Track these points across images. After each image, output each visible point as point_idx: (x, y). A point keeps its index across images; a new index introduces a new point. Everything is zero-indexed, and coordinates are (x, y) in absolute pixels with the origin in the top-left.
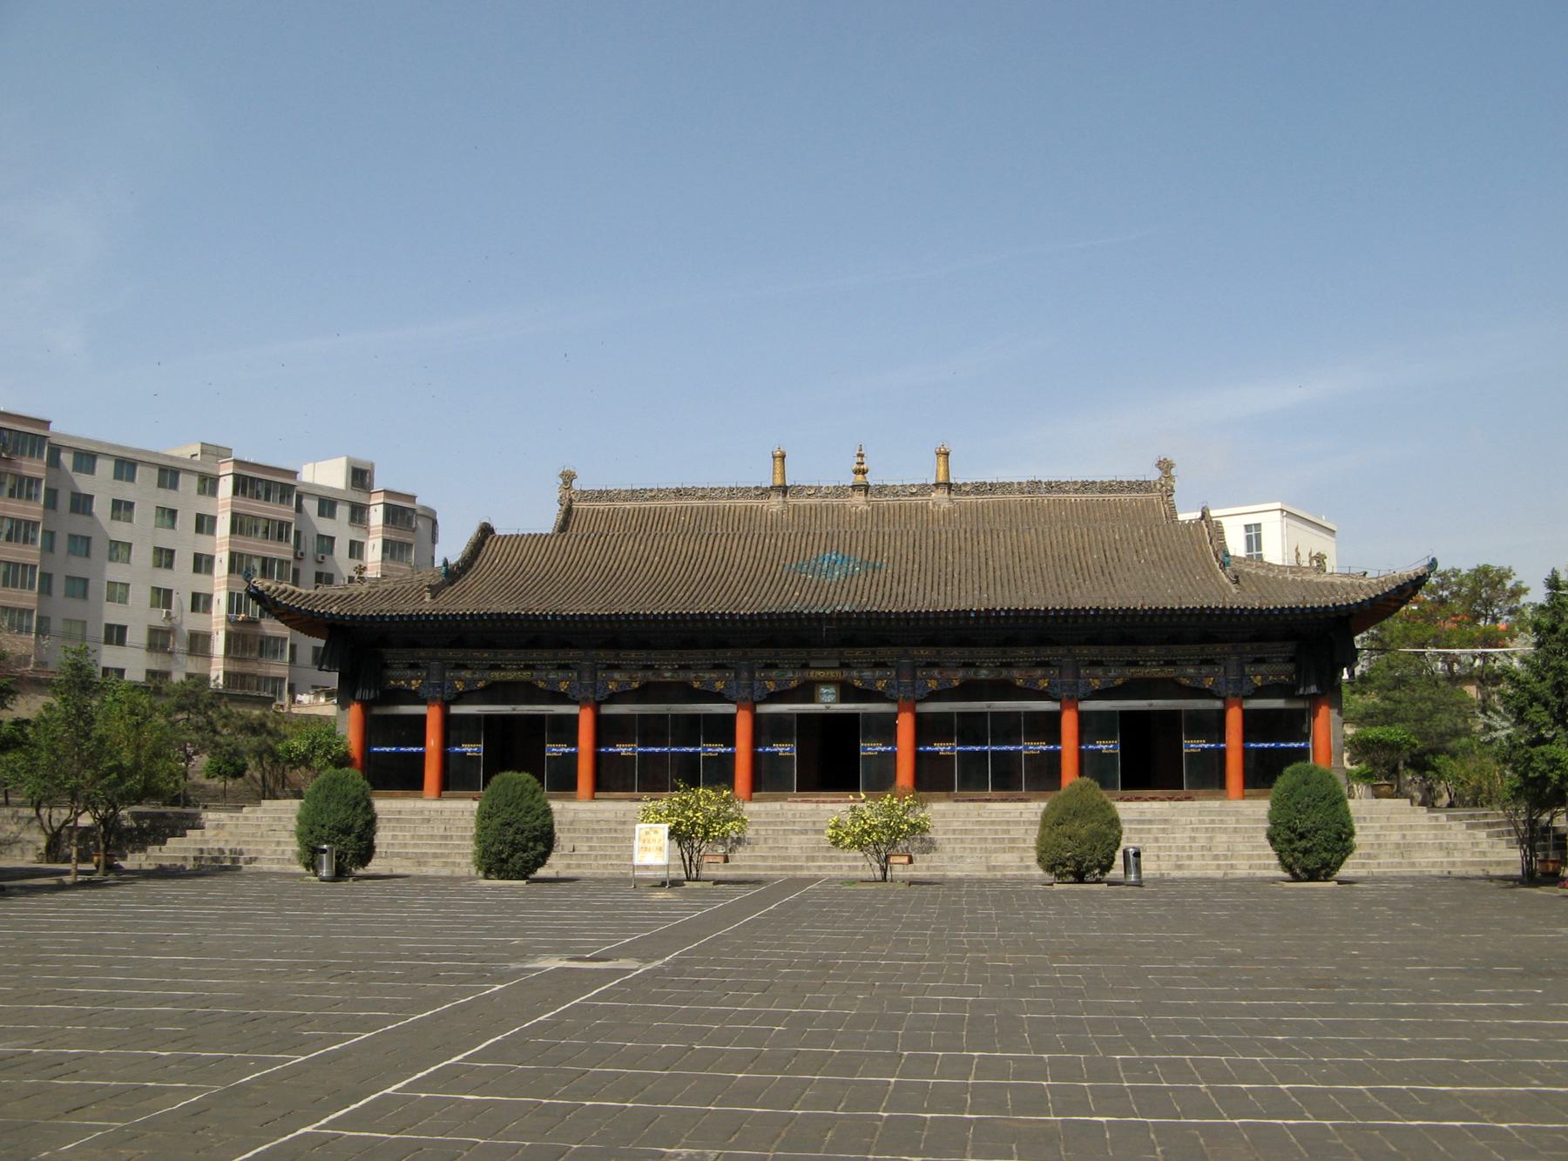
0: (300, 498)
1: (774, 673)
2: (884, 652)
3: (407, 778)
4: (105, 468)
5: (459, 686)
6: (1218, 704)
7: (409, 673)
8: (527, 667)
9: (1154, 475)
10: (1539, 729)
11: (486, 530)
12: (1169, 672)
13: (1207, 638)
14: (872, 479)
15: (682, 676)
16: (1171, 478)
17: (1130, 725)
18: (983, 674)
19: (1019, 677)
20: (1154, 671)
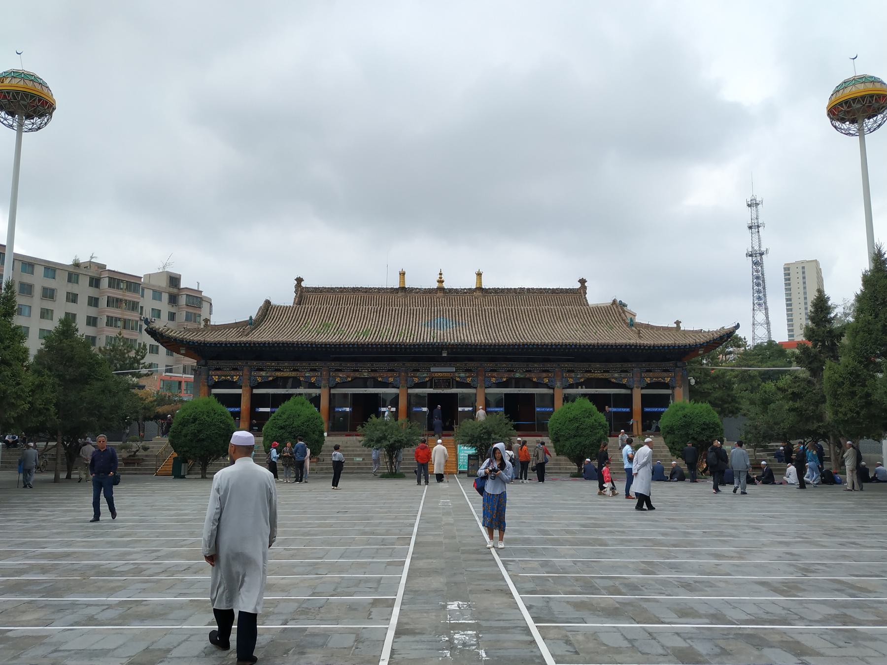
0: (143, 290)
1: (573, 375)
2: (471, 365)
3: (621, 423)
4: (39, 271)
5: (259, 379)
6: (551, 391)
8: (294, 370)
9: (578, 286)
11: (268, 303)
12: (606, 376)
13: (625, 360)
14: (446, 285)
15: (372, 375)
16: (585, 288)
17: (432, 400)
18: (518, 375)
19: (615, 376)
20: (599, 375)
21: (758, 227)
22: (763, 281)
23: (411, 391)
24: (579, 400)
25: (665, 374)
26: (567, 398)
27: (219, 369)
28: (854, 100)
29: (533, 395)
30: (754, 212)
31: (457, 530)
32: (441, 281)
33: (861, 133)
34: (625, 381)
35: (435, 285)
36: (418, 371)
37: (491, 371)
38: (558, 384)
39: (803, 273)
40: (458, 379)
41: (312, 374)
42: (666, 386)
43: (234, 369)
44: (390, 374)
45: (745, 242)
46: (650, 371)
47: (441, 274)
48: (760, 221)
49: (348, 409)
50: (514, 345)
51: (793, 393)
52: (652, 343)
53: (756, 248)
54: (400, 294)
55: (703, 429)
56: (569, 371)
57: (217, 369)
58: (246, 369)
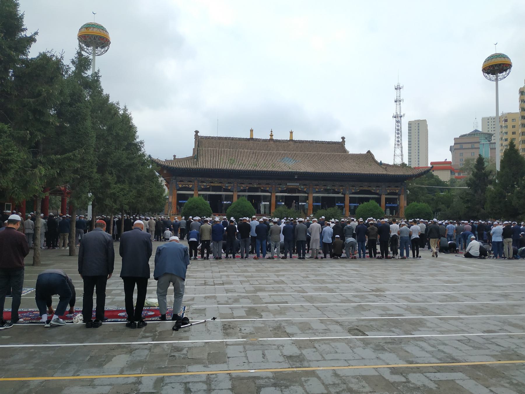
1: (354, 188)
2: (307, 182)
5: (202, 187)
6: (307, 195)
7: (189, 183)
8: (220, 183)
9: (341, 140)
10: (193, 245)
14: (274, 138)
15: (259, 186)
16: (345, 142)
19: (373, 189)
20: (366, 188)
21: (400, 101)
22: (401, 132)
23: (200, 193)
24: (371, 201)
25: (396, 188)
26: (239, 196)
27: (182, 181)
28: (496, 65)
29: (260, 196)
30: (398, 93)
32: (271, 136)
34: (378, 191)
35: (269, 138)
36: (281, 184)
38: (348, 192)
39: (418, 127)
41: (229, 185)
42: (395, 194)
43: (189, 181)
44: (267, 186)
45: (393, 109)
46: (390, 187)
49: (225, 202)
51: (468, 200)
53: (398, 113)
54: (251, 142)
55: (426, 215)
56: (353, 186)
57: (180, 181)
58: (196, 181)
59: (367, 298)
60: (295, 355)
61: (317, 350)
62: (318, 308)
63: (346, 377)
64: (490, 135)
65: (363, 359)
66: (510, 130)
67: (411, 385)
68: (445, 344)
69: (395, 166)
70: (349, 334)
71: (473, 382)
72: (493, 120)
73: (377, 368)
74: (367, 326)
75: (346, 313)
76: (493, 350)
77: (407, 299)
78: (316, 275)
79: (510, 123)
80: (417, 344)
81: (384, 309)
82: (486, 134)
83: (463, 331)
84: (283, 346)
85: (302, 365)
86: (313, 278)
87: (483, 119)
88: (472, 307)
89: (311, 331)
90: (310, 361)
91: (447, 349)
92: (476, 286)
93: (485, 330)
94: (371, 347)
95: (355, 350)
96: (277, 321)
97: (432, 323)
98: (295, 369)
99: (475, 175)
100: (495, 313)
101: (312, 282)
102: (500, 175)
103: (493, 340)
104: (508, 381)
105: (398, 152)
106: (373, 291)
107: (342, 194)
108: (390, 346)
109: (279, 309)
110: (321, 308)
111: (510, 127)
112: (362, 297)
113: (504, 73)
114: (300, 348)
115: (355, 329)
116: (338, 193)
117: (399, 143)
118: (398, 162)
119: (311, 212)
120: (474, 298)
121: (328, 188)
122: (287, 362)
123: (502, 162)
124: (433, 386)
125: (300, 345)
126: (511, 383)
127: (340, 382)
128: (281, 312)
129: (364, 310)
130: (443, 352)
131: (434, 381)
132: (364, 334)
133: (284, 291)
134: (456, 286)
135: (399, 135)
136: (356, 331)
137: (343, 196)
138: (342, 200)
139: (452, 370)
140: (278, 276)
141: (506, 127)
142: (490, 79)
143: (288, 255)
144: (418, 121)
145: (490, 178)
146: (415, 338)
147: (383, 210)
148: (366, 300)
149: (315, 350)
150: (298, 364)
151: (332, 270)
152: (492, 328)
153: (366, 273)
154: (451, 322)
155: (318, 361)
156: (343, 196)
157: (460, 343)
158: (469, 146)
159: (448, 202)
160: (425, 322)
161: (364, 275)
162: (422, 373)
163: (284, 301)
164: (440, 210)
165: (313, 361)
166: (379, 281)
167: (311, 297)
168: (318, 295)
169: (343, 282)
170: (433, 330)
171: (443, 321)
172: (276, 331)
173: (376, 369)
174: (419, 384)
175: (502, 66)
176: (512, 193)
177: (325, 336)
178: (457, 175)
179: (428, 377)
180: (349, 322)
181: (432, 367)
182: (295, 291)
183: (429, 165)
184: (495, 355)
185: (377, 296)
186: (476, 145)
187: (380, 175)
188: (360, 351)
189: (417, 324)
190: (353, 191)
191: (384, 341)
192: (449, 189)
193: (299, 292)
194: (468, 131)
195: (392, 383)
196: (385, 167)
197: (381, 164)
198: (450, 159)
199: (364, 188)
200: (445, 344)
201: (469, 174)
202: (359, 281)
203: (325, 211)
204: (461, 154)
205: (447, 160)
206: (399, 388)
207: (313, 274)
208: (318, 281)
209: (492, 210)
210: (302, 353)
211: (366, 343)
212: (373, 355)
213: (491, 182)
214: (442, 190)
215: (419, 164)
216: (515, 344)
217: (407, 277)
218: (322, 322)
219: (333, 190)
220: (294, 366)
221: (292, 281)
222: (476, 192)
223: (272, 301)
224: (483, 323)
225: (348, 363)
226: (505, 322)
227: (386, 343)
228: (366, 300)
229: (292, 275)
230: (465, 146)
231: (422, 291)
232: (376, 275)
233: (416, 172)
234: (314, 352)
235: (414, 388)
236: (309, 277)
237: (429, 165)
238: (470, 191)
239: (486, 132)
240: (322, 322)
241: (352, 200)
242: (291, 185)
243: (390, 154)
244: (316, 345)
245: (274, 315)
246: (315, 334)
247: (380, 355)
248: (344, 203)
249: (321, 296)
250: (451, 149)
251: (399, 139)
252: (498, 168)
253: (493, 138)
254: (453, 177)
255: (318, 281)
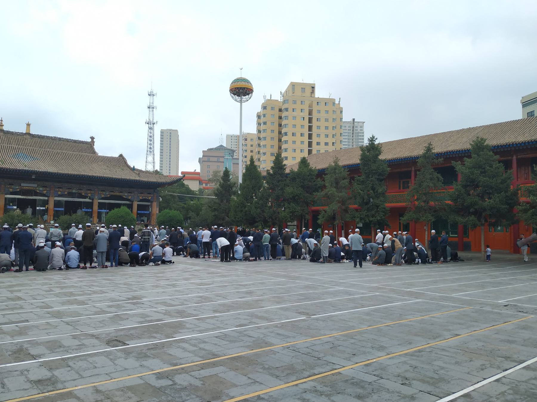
1: (104, 193)
6: (46, 198)
9: (90, 140)
19: (125, 195)
20: (118, 194)
21: (153, 108)
24: (122, 207)
25: (149, 195)
28: (241, 88)
29: (36, 200)
30: (151, 99)
31: (501, 183)
33: (241, 102)
34: (130, 198)
36: (13, 185)
37: (58, 188)
38: (96, 197)
40: (38, 191)
42: (148, 201)
46: (142, 193)
47: (2, 121)
48: (154, 105)
50: (100, 177)
52: (165, 181)
56: (102, 191)
59: (124, 307)
60: (45, 378)
61: (72, 369)
62: (68, 323)
63: (109, 391)
64: (233, 151)
65: (126, 369)
66: (249, 148)
67: (178, 387)
68: (205, 342)
69: (147, 172)
70: (108, 347)
71: (232, 373)
72: (235, 138)
73: (141, 376)
74: (127, 336)
75: (101, 325)
76: (247, 342)
77: (164, 303)
78: (62, 288)
79: (249, 143)
80: (179, 346)
81: (144, 316)
82: (230, 150)
83: (219, 328)
84: (29, 371)
85: (55, 387)
86: (58, 291)
87: (227, 136)
88: (224, 305)
89: (62, 349)
90: (65, 382)
91: (207, 347)
92: (226, 286)
93: (238, 324)
94: (133, 356)
95: (116, 362)
96: (17, 344)
97: (191, 324)
98: (47, 394)
99: (222, 186)
100: (244, 309)
101: (57, 295)
102: (242, 187)
103: (245, 333)
104: (262, 366)
105: (150, 159)
106: (129, 299)
107: (90, 199)
108: (152, 352)
109: (17, 329)
110: (72, 322)
111: (249, 145)
112: (118, 307)
113: (247, 97)
114: (50, 369)
115: (113, 340)
116: (85, 197)
117: (152, 150)
118: (150, 168)
119: (52, 218)
120: (225, 298)
121: (74, 191)
122: (35, 387)
123: (244, 175)
124: (198, 383)
125: (50, 366)
126: (264, 368)
127: (103, 397)
128: (21, 332)
129: (122, 319)
130: (204, 349)
131: (199, 378)
132: (125, 344)
133: (21, 308)
134: (209, 287)
135: (152, 142)
136: (115, 342)
137: (91, 201)
138: (90, 205)
139: (214, 365)
140: (12, 292)
141: (246, 145)
142: (236, 100)
143: (24, 268)
144: (170, 130)
145: (234, 189)
146: (176, 340)
147: (135, 216)
148: (123, 309)
149: (69, 369)
150: (50, 388)
151: (81, 281)
152: (243, 322)
153: (120, 282)
154: (208, 321)
155: (74, 380)
156: (91, 201)
157: (218, 339)
158: (215, 159)
159: (197, 210)
160: (184, 324)
161: (117, 284)
162: (187, 373)
163: (23, 319)
164: (190, 218)
165: (68, 381)
166: (134, 289)
167: (59, 312)
168: (66, 309)
169: (95, 292)
170: (193, 331)
171: (200, 321)
172: (17, 355)
173: (141, 378)
174: (185, 384)
175: (246, 89)
176: (251, 204)
177: (80, 352)
178: (204, 185)
179: (193, 376)
180: (106, 334)
181: (196, 365)
182: (37, 307)
183: (180, 174)
184: (249, 346)
185: (134, 304)
186: (221, 159)
187: (132, 180)
188: (122, 362)
189: (178, 327)
190: (103, 196)
191: (147, 348)
192: (198, 198)
193: (41, 307)
194: (214, 146)
195: (159, 389)
196: (137, 173)
197: (134, 169)
198: (198, 170)
199: (115, 194)
200: (205, 342)
201: (216, 184)
202: (113, 291)
203: (69, 217)
204: (209, 166)
205: (197, 171)
206: (166, 392)
207: (57, 287)
208: (65, 294)
209: (235, 218)
210: (53, 375)
211: (127, 353)
212: (137, 364)
213: (235, 193)
214: (192, 199)
215: (170, 173)
216: (263, 333)
217: (163, 283)
218: (74, 337)
219: (80, 193)
220: (45, 391)
221: (31, 296)
222: (222, 201)
223: (7, 321)
224: (235, 319)
225: (110, 376)
226: (253, 315)
227: (148, 349)
228: (123, 309)
229: (31, 290)
230: (212, 159)
231: (179, 295)
232: (130, 283)
233: (168, 180)
234: (69, 371)
235: (181, 389)
236: (52, 291)
237: (180, 174)
238: (217, 201)
239: (230, 148)
240: (74, 337)
241: (101, 206)
242: (26, 185)
243: (143, 161)
244: (71, 363)
245: (12, 337)
246: (67, 352)
247: (144, 363)
248: (92, 209)
249: (70, 310)
250: (200, 160)
251: (152, 146)
252: (240, 181)
253: (235, 154)
254: (202, 187)
255: (65, 294)
